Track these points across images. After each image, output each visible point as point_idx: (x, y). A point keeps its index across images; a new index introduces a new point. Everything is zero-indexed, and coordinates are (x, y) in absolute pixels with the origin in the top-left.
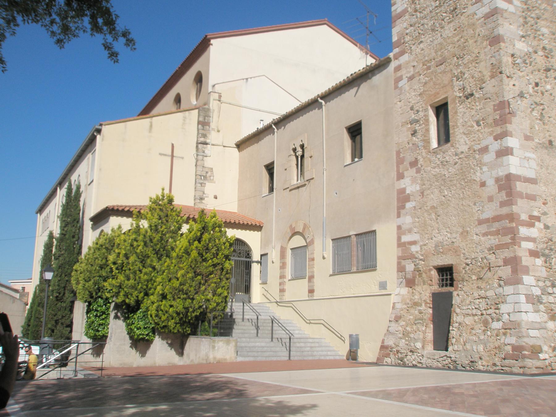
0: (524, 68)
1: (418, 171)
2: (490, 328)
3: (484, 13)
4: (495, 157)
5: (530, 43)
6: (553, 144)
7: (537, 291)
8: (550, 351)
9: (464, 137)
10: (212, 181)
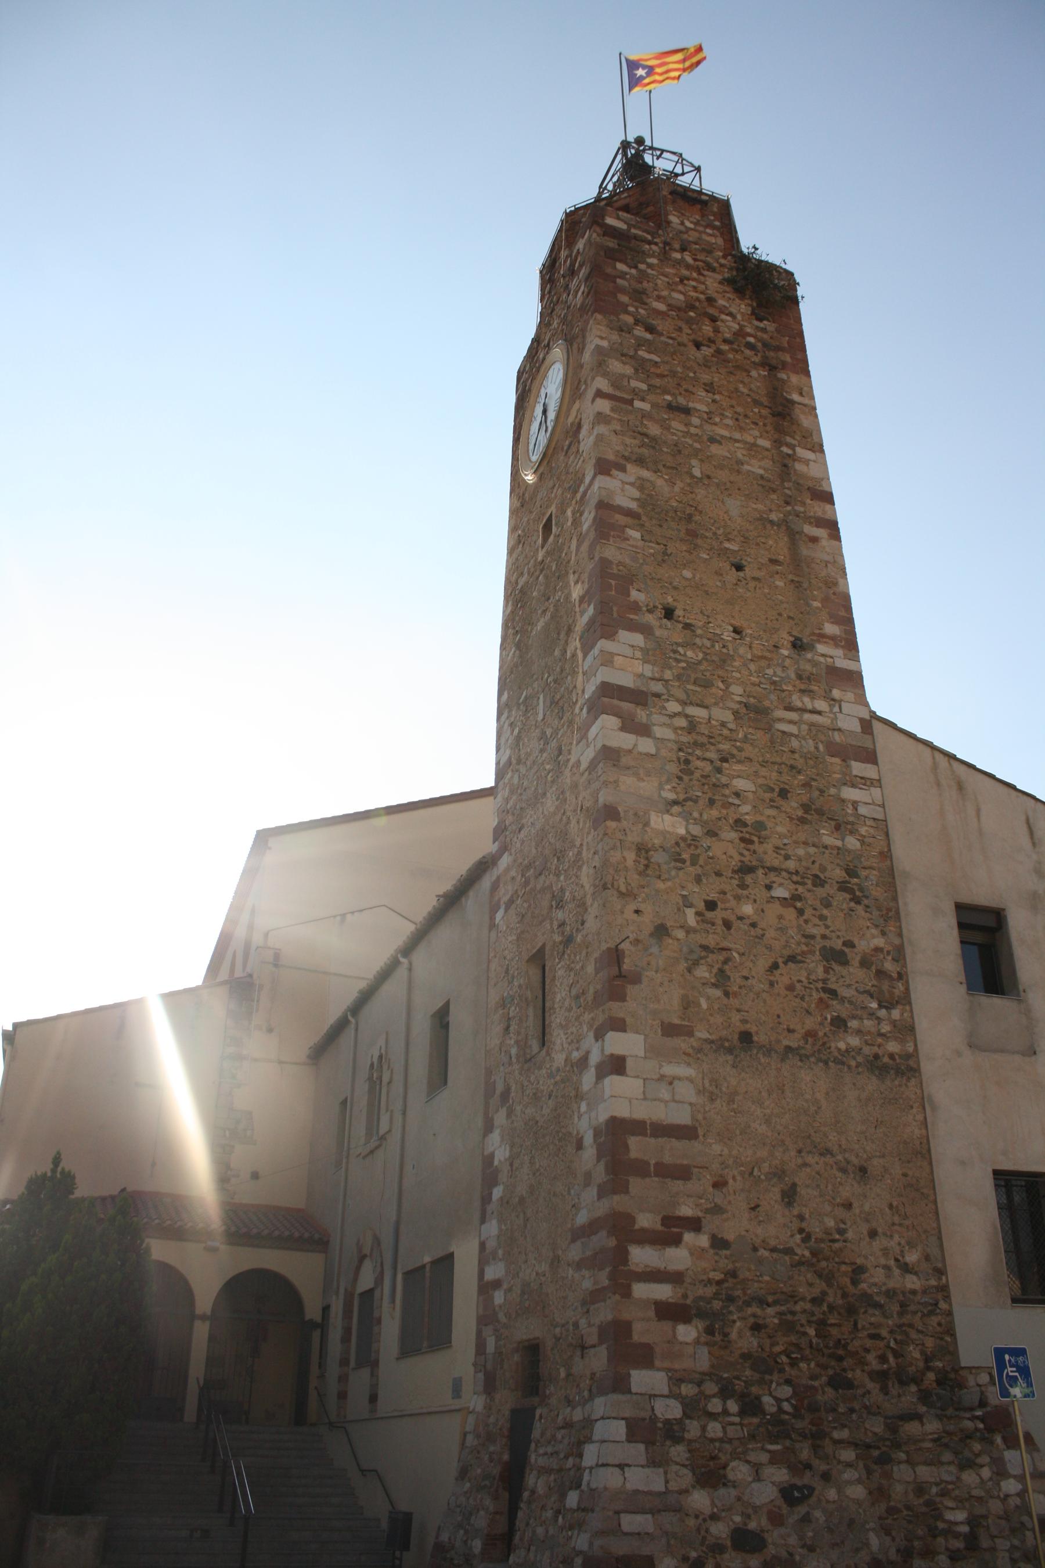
0: (673, 873)
4: (594, 1079)
5: (696, 815)
6: (755, 1038)
7: (670, 1410)
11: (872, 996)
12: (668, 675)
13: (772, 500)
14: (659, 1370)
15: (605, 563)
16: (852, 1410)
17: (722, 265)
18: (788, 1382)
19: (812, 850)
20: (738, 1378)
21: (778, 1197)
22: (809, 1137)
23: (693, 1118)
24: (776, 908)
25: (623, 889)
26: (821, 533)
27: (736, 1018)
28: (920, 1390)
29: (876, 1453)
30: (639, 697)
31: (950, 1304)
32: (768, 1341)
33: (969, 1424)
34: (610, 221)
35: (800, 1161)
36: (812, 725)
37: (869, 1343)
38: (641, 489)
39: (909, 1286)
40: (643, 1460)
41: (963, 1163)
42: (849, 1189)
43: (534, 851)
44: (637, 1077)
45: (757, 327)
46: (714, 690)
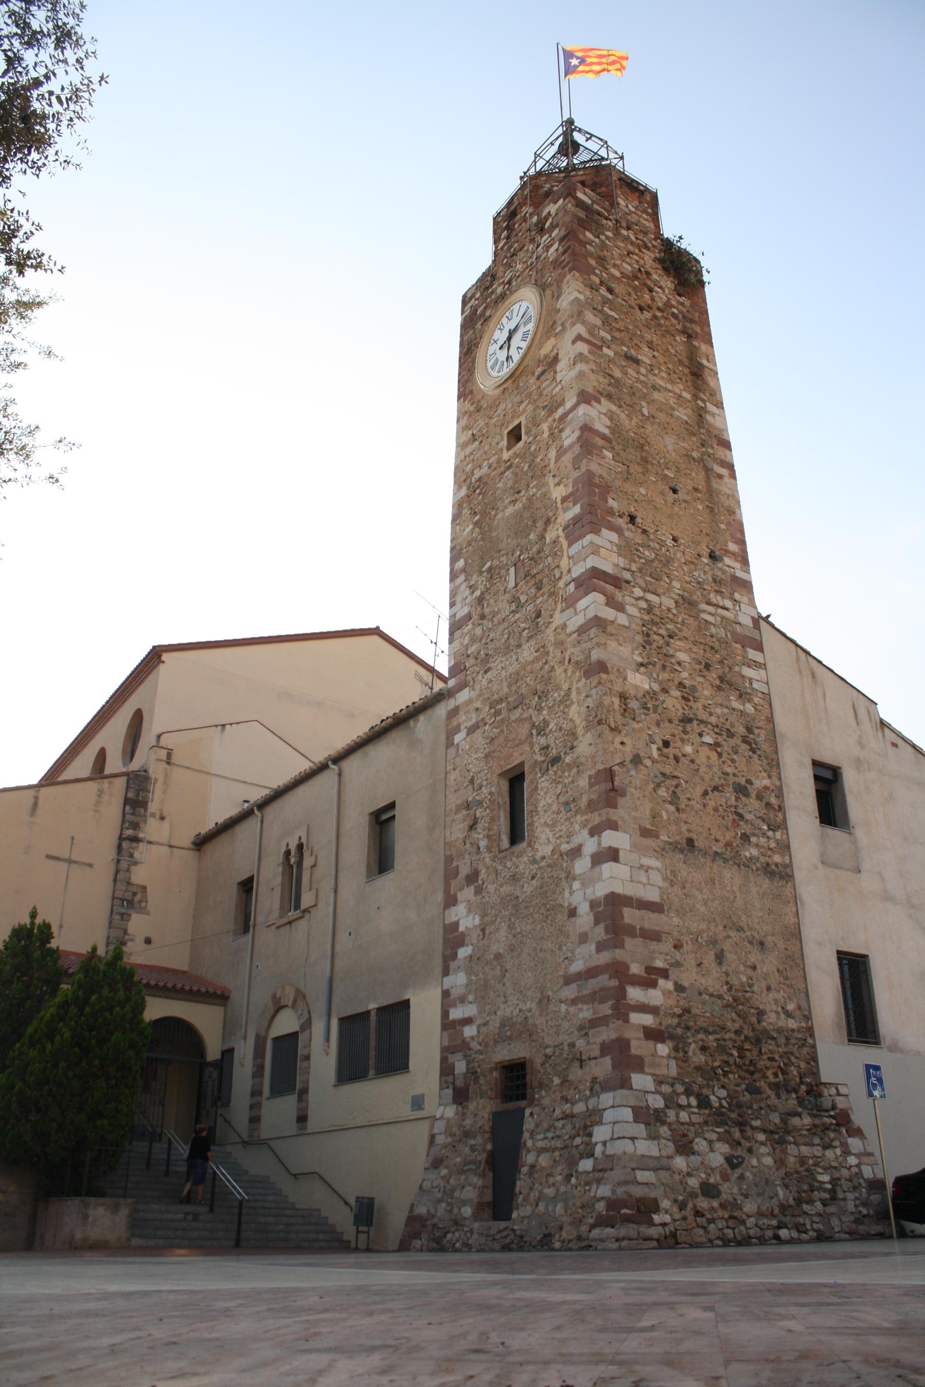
0: (643, 717)
1: (478, 891)
2: (577, 1171)
3: (577, 625)
4: (590, 865)
5: (655, 675)
6: (696, 844)
7: (657, 1102)
8: (675, 1209)
9: (547, 830)
10: (144, 911)
11: (763, 821)
12: (634, 567)
13: (693, 442)
14: (647, 1074)
15: (590, 474)
16: (761, 1108)
17: (654, 246)
18: (723, 1087)
19: (726, 710)
20: (694, 1082)
21: (713, 958)
22: (730, 917)
23: (661, 897)
24: (705, 751)
25: (613, 725)
26: (724, 472)
27: (684, 828)
28: (798, 1098)
29: (777, 1137)
30: (616, 582)
31: (814, 1040)
32: (710, 1059)
33: (827, 1120)
34: (580, 195)
35: (725, 934)
36: (723, 618)
37: (768, 1063)
38: (611, 419)
39: (790, 1026)
40: (644, 1135)
41: (819, 944)
42: (755, 956)
43: (506, 689)
44: (626, 865)
45: (678, 301)
46: (662, 583)
